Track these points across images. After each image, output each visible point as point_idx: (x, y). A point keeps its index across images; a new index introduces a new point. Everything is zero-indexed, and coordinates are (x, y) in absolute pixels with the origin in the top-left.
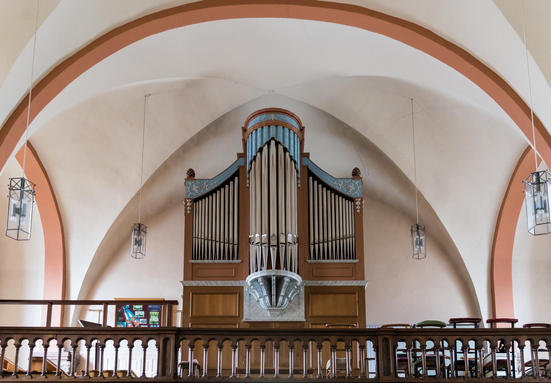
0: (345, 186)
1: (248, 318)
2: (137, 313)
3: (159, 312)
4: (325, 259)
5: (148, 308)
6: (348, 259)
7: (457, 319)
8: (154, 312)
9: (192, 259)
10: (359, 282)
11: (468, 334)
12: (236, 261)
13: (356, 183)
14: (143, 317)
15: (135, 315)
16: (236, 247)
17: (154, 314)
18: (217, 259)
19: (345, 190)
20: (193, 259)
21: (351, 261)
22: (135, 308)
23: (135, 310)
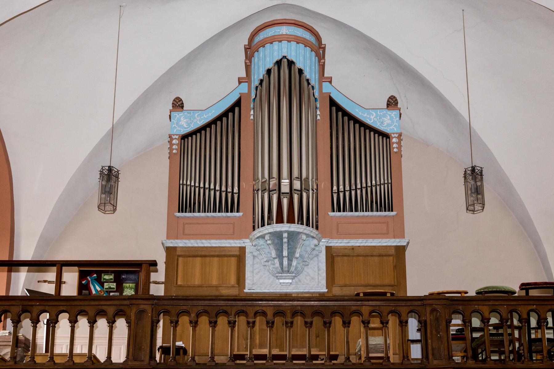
0: (378, 118)
1: (252, 288)
2: (106, 285)
3: (135, 284)
4: (352, 211)
5: (121, 278)
6: (382, 211)
7: (531, 283)
8: (129, 284)
9: (178, 212)
10: (398, 240)
11: (546, 303)
12: (235, 214)
13: (393, 115)
14: (115, 290)
15: (103, 288)
16: (236, 196)
17: (129, 286)
18: (211, 212)
19: (379, 124)
20: (179, 212)
21: (387, 213)
22: (105, 279)
23: (105, 281)
